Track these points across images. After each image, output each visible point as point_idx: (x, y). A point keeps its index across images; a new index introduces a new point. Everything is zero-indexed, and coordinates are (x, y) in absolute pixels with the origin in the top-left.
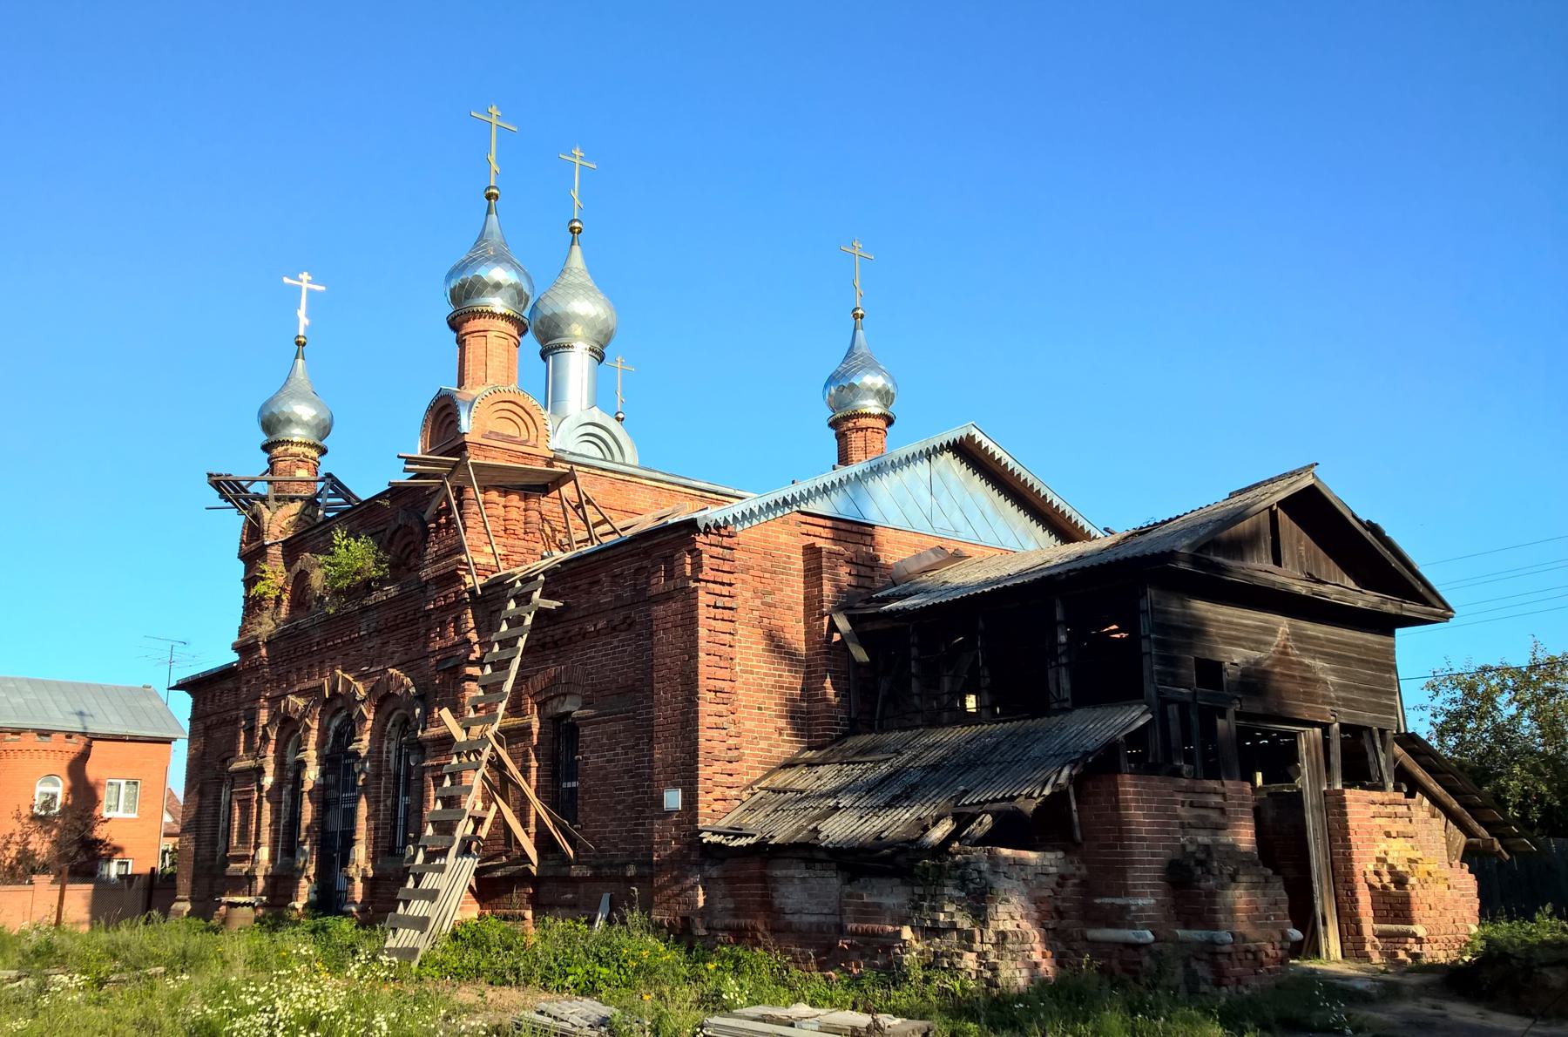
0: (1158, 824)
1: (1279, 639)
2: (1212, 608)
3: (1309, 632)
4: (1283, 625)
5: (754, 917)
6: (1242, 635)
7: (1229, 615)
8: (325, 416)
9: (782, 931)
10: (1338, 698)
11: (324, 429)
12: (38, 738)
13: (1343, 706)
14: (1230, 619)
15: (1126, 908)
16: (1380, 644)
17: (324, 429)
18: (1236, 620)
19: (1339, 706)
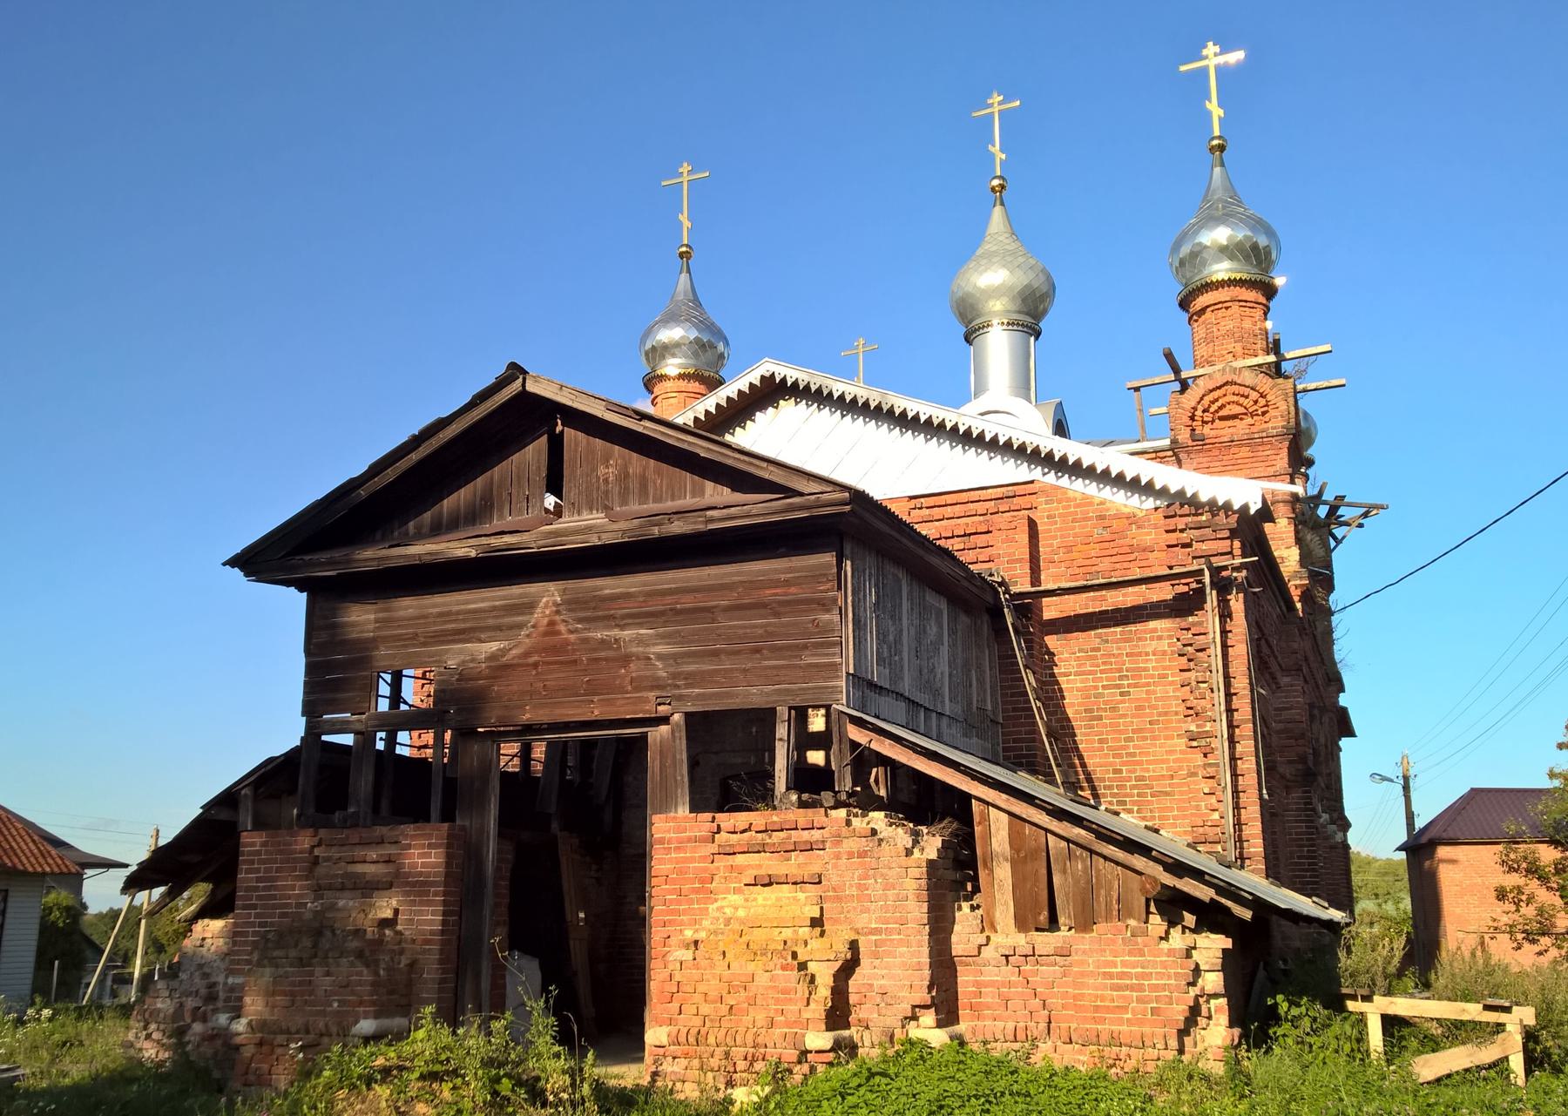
0: (276, 888)
1: (541, 615)
2: (415, 603)
3: (607, 592)
4: (548, 594)
5: (1362, 1020)
6: (468, 625)
7: (444, 605)
8: (1039, 283)
9: (1527, 1042)
10: (675, 676)
11: (1258, 256)
12: (1459, 834)
13: (688, 686)
14: (445, 609)
15: (442, 974)
16: (790, 570)
17: (1258, 256)
18: (456, 608)
19: (678, 687)
